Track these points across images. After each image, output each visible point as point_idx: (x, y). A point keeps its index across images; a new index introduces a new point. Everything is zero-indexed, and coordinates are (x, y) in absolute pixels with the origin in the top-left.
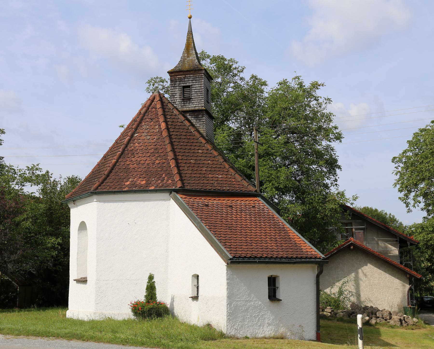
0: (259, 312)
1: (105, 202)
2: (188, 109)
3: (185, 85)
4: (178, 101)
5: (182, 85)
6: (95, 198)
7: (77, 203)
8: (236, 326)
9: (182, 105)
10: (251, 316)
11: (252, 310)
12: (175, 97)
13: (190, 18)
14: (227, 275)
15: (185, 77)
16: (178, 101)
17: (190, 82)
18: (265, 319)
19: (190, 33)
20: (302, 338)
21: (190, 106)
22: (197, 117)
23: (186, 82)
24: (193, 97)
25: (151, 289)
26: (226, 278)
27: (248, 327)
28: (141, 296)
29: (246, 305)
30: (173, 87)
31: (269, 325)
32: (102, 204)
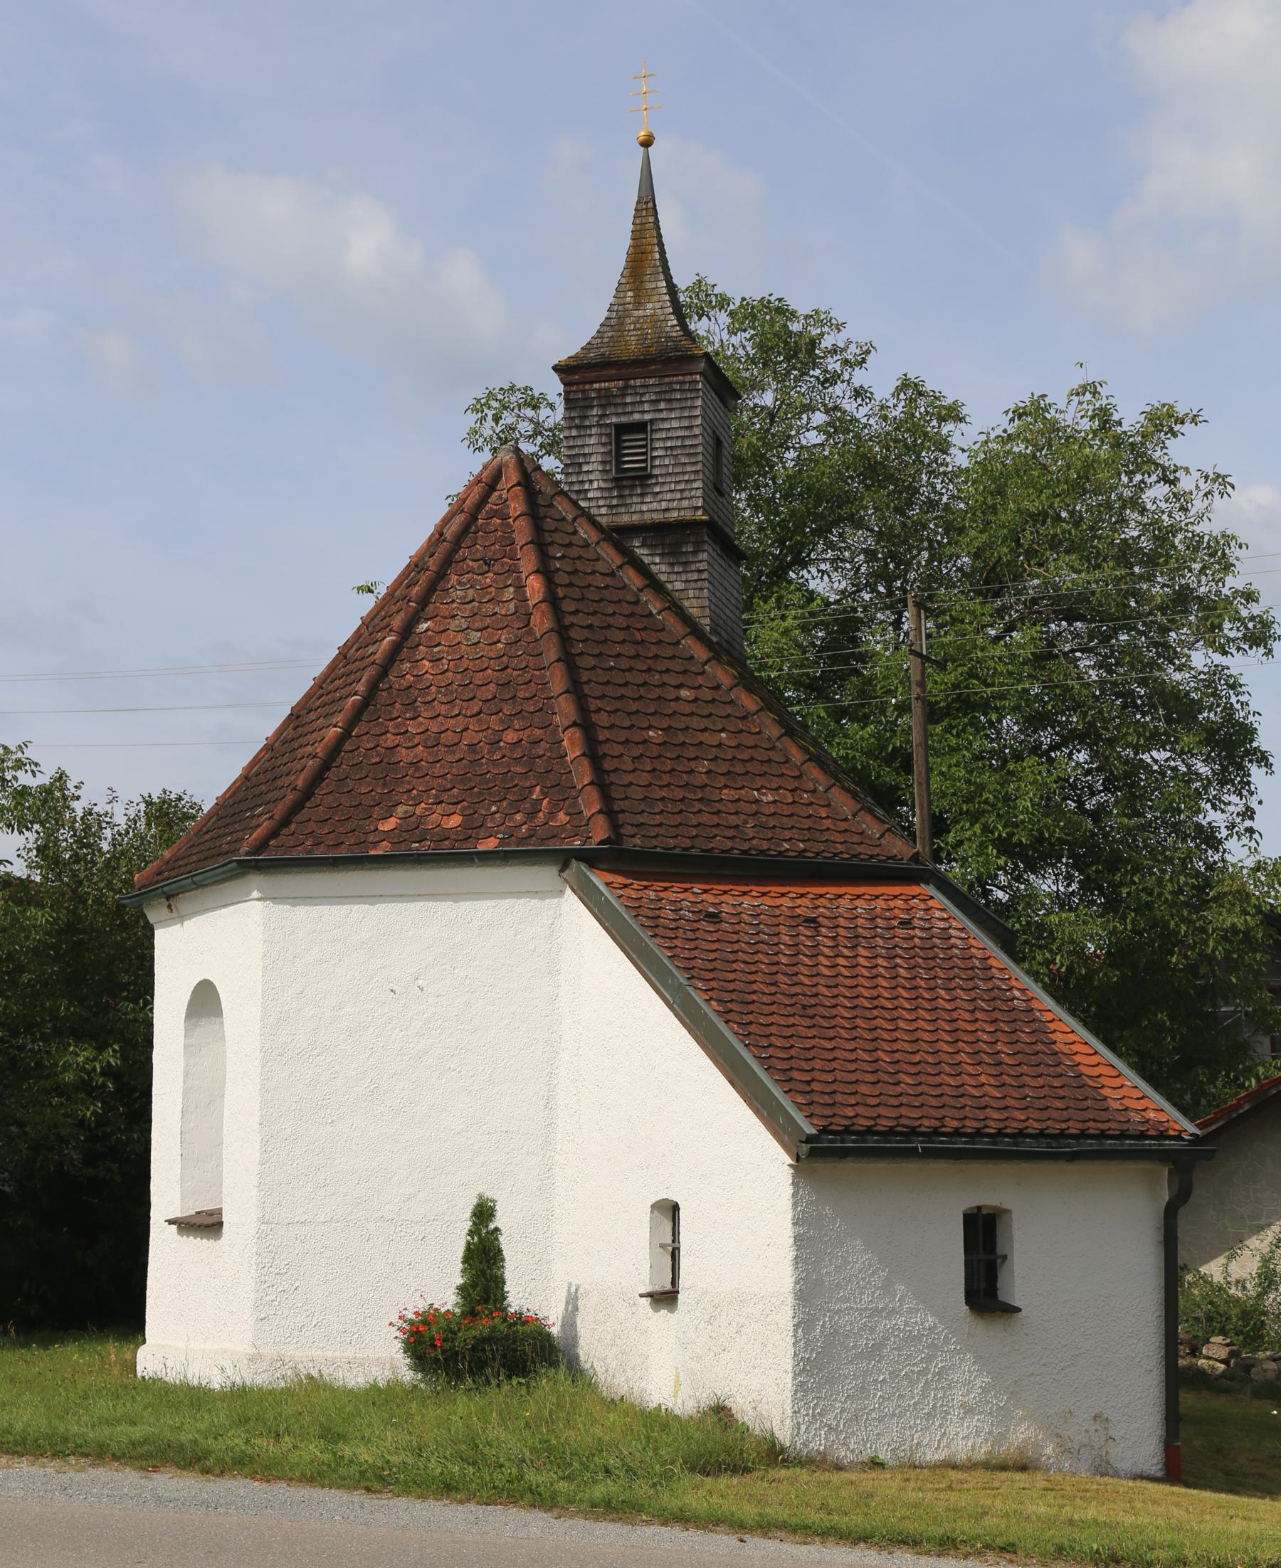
0: (929, 1359)
1: (294, 900)
2: (635, 517)
3: (624, 419)
4: (595, 485)
5: (614, 420)
6: (255, 885)
7: (183, 903)
8: (832, 1416)
9: (615, 502)
10: (894, 1374)
11: (899, 1349)
12: (585, 468)
13: (647, 143)
14: (795, 1204)
15: (626, 387)
16: (595, 485)
17: (646, 407)
18: (950, 1387)
19: (647, 207)
20: (1103, 1469)
21: (645, 508)
22: (673, 555)
23: (629, 409)
24: (656, 472)
25: (484, 1258)
26: (790, 1215)
27: (881, 1420)
28: (442, 1289)
29: (872, 1330)
30: (577, 427)
31: (969, 1410)
32: (281, 911)
